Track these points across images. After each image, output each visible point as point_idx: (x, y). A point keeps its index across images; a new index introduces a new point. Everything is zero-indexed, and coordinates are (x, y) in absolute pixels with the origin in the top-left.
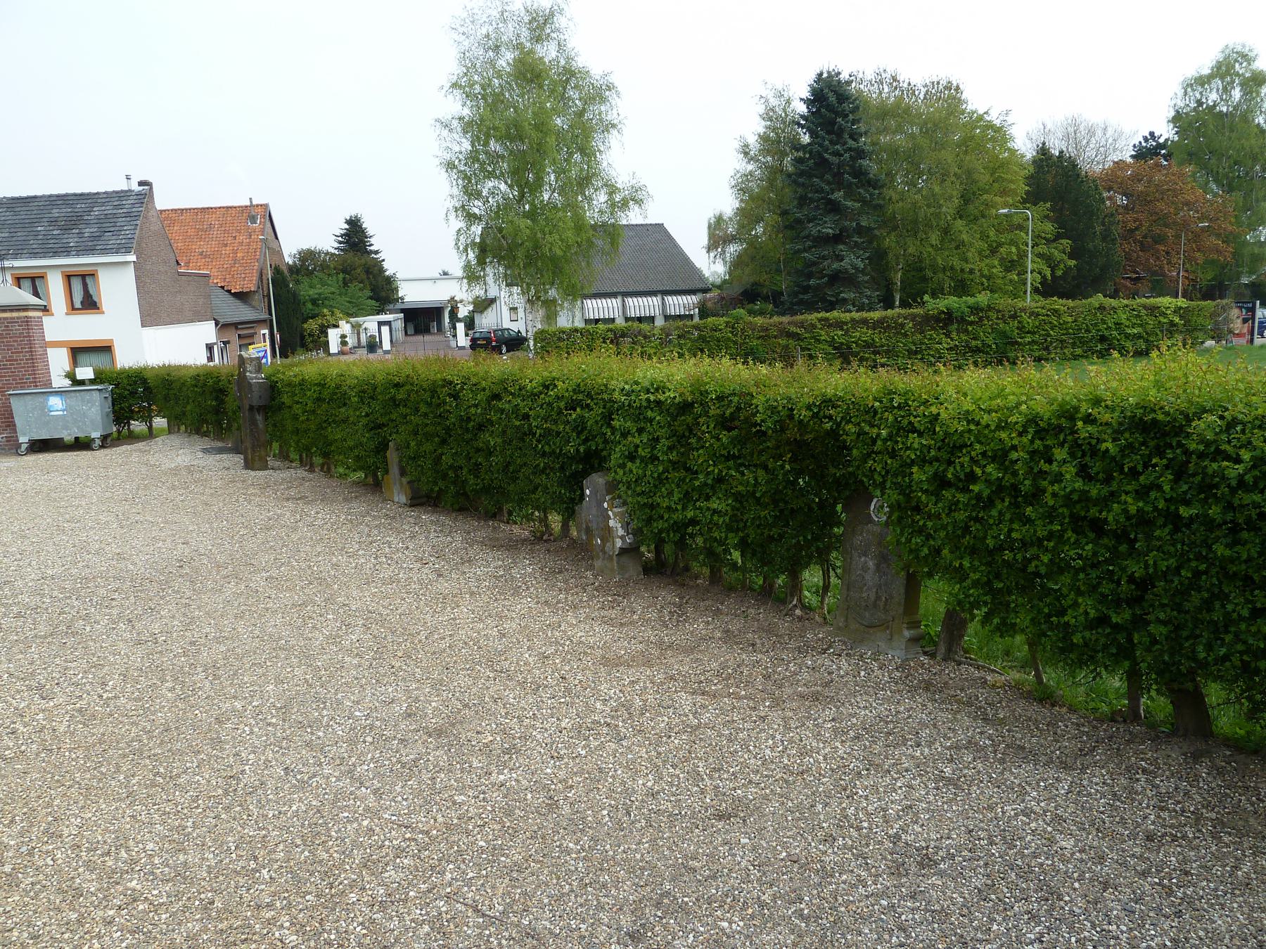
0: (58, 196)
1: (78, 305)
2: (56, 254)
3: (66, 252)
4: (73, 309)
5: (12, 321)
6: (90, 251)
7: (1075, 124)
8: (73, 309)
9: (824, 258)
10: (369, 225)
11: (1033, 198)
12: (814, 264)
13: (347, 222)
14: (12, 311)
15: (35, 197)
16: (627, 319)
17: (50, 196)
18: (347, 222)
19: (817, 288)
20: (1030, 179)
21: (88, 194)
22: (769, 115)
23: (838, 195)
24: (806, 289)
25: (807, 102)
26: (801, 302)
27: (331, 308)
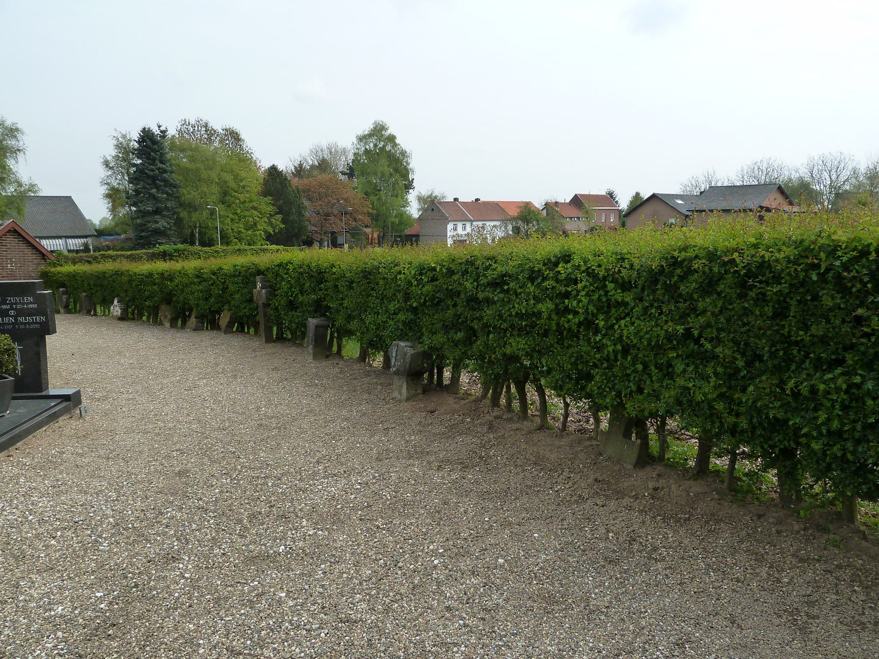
7: (185, 123)
9: (149, 222)
11: (265, 193)
12: (144, 225)
16: (69, 251)
19: (147, 237)
20: (266, 182)
22: (119, 146)
23: (154, 191)
24: (142, 238)
25: (139, 142)
26: (137, 244)
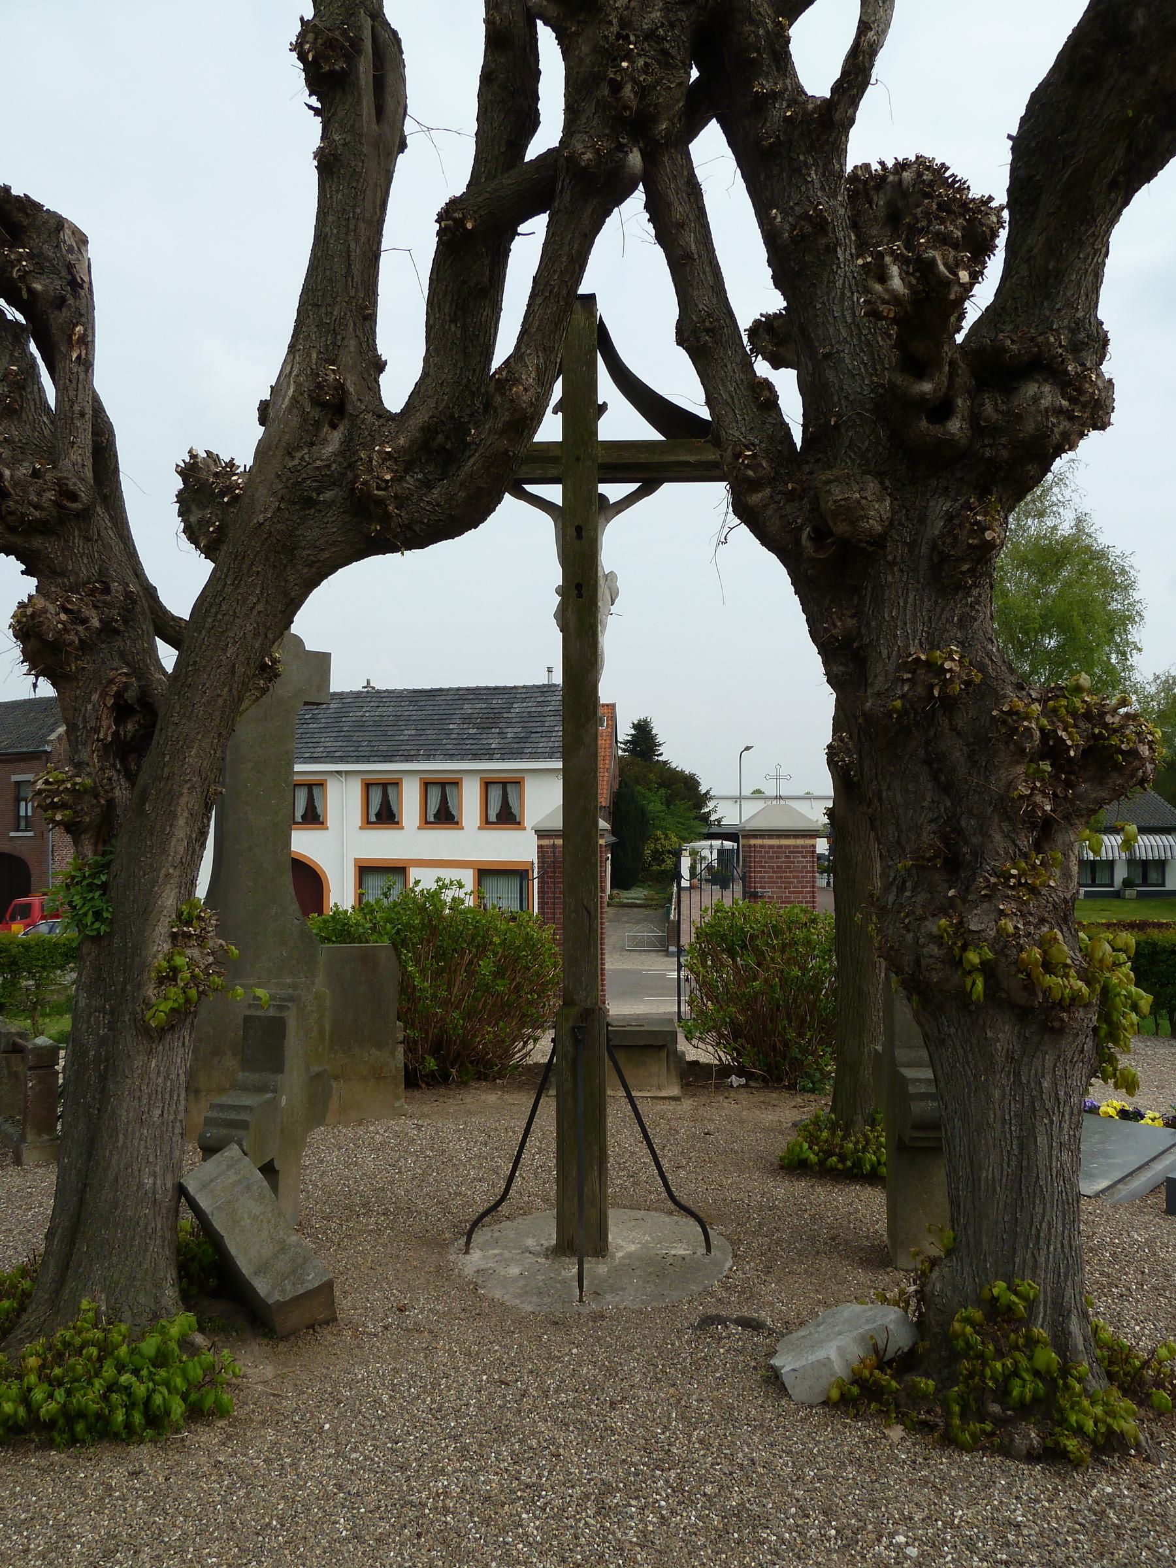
0: (467, 689)
1: (492, 818)
2: (476, 757)
3: (489, 755)
4: (486, 823)
5: (795, 850)
6: (518, 754)
8: (486, 823)
10: (659, 730)
13: (635, 727)
14: (796, 837)
15: (441, 690)
17: (459, 689)
18: (635, 727)
21: (505, 688)
27: (664, 829)
